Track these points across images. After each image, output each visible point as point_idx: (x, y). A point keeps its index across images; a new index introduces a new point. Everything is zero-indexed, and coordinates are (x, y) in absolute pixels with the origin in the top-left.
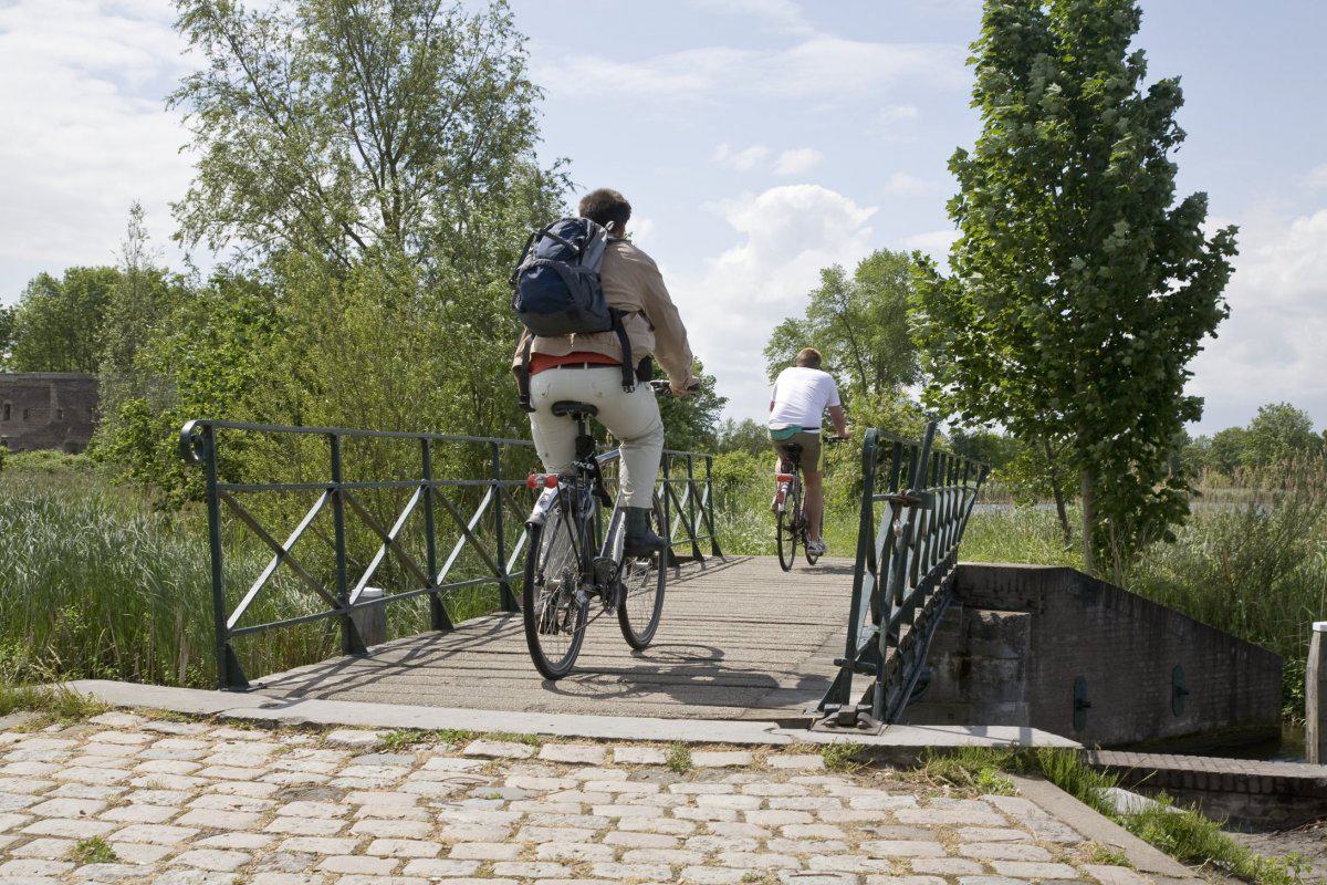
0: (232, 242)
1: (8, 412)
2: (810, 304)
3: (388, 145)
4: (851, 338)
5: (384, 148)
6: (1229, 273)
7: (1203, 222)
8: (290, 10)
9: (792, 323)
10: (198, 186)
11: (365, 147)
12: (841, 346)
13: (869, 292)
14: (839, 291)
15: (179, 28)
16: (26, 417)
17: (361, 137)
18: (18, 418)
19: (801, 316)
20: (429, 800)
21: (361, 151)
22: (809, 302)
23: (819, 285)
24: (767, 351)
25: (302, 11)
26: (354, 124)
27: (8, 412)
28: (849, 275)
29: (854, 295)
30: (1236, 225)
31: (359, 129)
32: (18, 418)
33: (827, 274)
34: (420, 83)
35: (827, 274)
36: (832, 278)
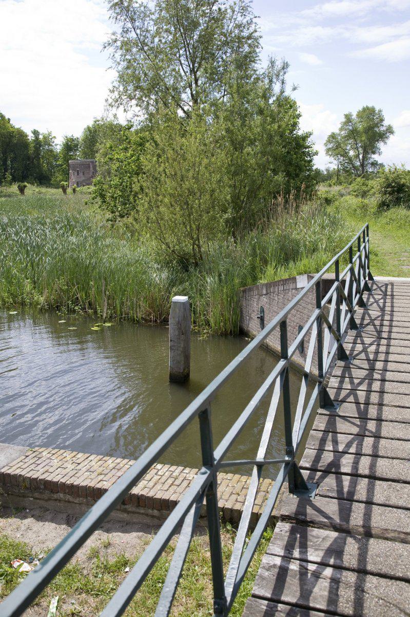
0: (133, 108)
1: (78, 173)
2: (340, 127)
3: (193, 65)
4: (355, 138)
5: (191, 66)
6: (41, 137)
7: (385, 143)
8: (152, 6)
9: (333, 133)
10: (116, 84)
11: (184, 67)
12: (351, 141)
13: (361, 122)
14: (351, 122)
15: (279, 65)
16: (83, 174)
17: (183, 62)
18: (81, 174)
19: (337, 131)
20: (9, 464)
21: (184, 68)
22: (340, 126)
23: (344, 120)
24: (325, 144)
25: (159, 5)
26: (180, 57)
27: (78, 173)
28: (354, 116)
29: (356, 123)
30: (395, 129)
31: (182, 58)
32: (81, 174)
33: (346, 116)
34: (207, 39)
35: (346, 116)
36: (348, 118)
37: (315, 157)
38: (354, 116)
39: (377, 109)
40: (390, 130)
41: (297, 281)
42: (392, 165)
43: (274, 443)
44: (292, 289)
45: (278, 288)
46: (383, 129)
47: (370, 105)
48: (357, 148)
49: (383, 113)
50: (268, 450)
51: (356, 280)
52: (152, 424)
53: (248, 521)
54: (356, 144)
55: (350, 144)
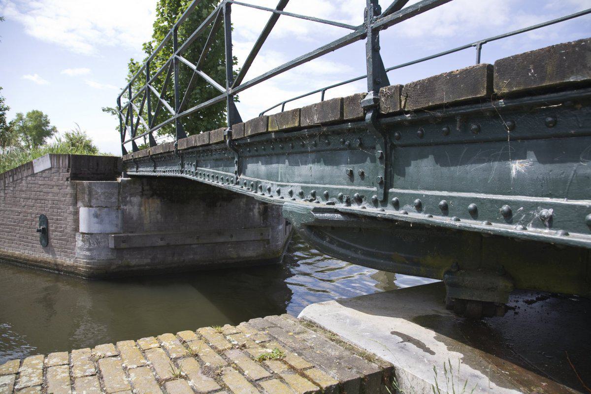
29: (26, 121)
37: (6, 112)
38: (25, 117)
39: (44, 114)
40: (54, 129)
41: (34, 165)
42: (75, 131)
43: (82, 346)
44: (27, 177)
45: (5, 181)
46: (49, 128)
47: (39, 110)
48: (28, 141)
49: (48, 118)
50: (108, 338)
51: (132, 125)
52: (508, 131)
53: (504, 389)
54: (27, 137)
55: (21, 137)
